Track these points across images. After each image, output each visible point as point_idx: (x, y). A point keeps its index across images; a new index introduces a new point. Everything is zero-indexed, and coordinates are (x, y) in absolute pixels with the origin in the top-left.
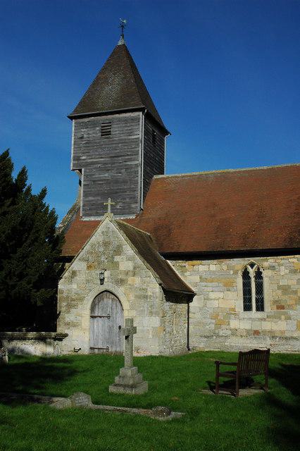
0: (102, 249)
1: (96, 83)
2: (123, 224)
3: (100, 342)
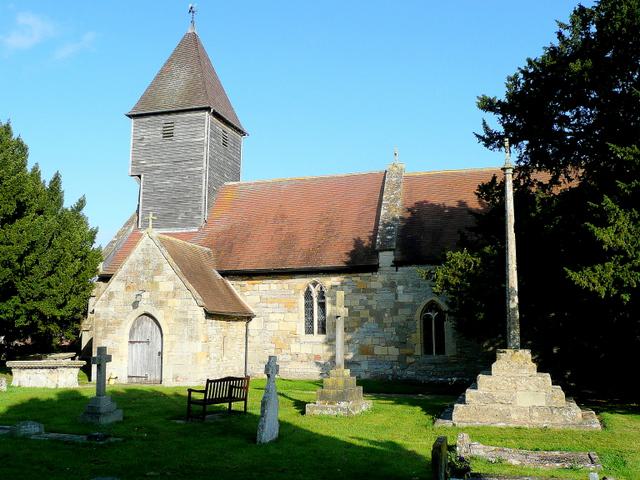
0: (141, 268)
1: (159, 77)
2: (169, 241)
3: (139, 369)
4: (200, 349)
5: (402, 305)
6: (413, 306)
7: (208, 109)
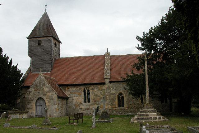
4: (57, 107)
5: (112, 94)
6: (115, 94)
7: (52, 36)
